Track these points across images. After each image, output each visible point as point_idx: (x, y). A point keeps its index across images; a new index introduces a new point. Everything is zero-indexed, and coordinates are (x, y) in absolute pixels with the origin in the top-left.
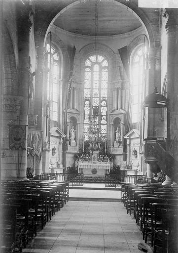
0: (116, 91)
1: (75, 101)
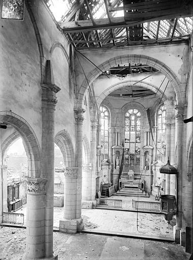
0: (146, 133)
1: (119, 138)
